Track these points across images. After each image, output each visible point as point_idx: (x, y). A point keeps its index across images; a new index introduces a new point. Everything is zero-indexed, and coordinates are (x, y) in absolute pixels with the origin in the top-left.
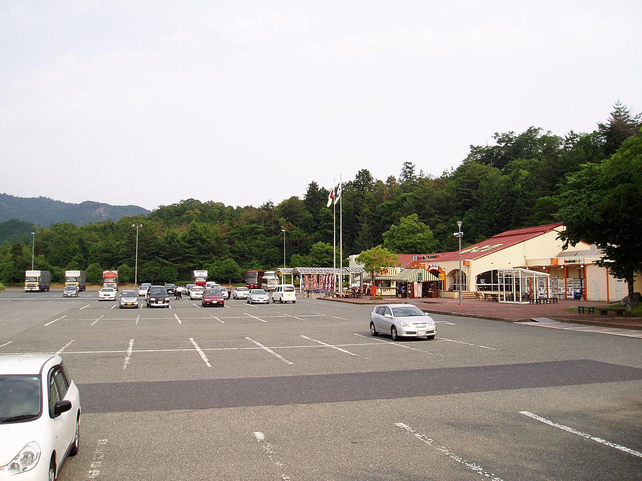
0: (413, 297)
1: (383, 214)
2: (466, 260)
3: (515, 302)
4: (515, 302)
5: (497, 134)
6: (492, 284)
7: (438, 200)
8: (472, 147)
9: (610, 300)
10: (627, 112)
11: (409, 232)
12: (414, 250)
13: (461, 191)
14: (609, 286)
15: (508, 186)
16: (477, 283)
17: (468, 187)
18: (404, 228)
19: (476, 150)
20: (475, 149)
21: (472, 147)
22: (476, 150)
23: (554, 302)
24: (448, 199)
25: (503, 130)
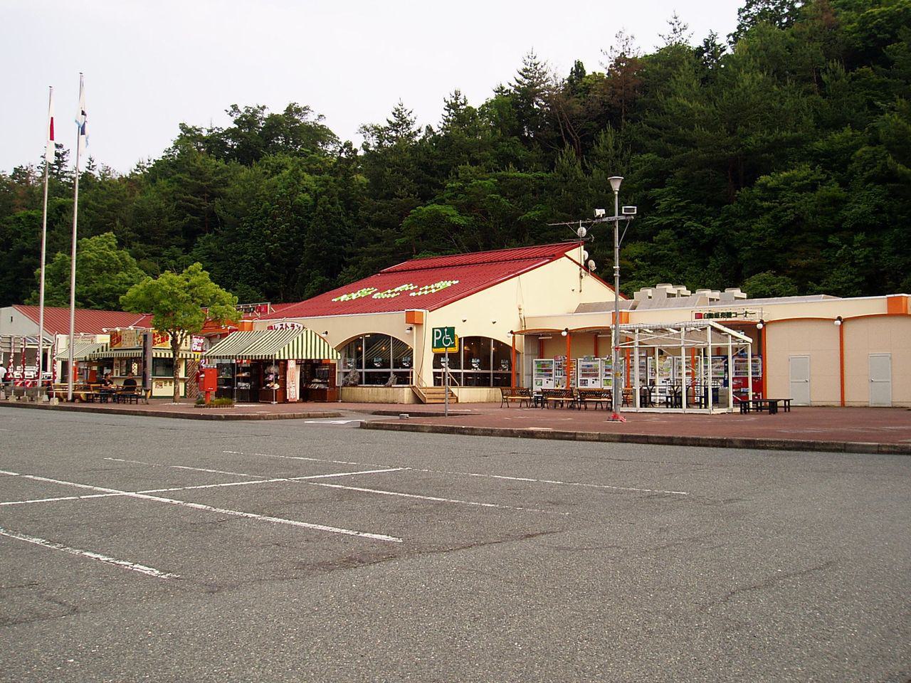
0: (285, 401)
1: (17, 234)
2: (245, 321)
3: (685, 409)
4: (684, 409)
5: (235, 107)
6: (462, 371)
7: (140, 213)
8: (183, 127)
9: (846, 404)
10: (544, 73)
11: (99, 270)
12: (114, 305)
13: (183, 200)
14: (845, 373)
15: (291, 194)
16: (434, 368)
17: (196, 194)
18: (90, 260)
19: (189, 135)
20: (189, 131)
21: (183, 127)
22: (189, 135)
23: (131, 401)
24: (160, 213)
25: (246, 102)
